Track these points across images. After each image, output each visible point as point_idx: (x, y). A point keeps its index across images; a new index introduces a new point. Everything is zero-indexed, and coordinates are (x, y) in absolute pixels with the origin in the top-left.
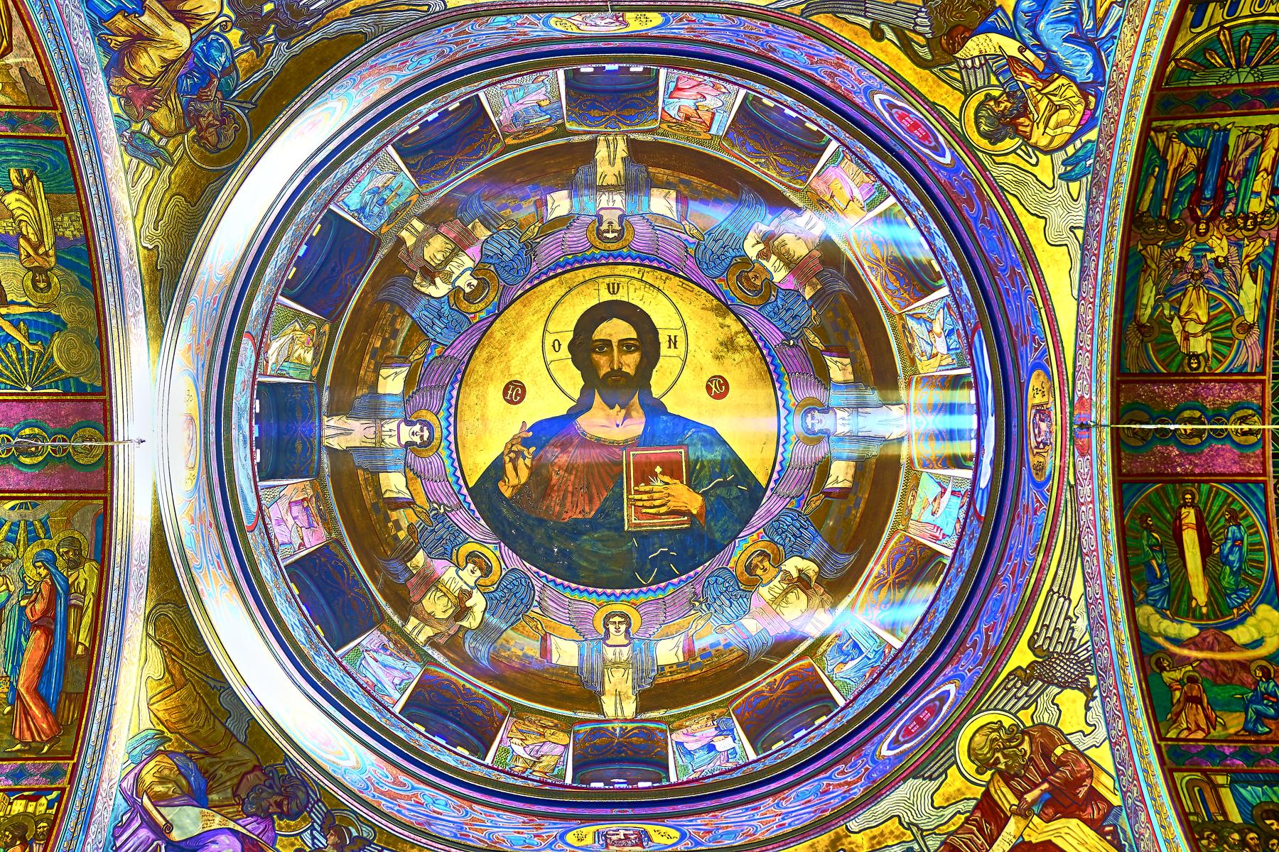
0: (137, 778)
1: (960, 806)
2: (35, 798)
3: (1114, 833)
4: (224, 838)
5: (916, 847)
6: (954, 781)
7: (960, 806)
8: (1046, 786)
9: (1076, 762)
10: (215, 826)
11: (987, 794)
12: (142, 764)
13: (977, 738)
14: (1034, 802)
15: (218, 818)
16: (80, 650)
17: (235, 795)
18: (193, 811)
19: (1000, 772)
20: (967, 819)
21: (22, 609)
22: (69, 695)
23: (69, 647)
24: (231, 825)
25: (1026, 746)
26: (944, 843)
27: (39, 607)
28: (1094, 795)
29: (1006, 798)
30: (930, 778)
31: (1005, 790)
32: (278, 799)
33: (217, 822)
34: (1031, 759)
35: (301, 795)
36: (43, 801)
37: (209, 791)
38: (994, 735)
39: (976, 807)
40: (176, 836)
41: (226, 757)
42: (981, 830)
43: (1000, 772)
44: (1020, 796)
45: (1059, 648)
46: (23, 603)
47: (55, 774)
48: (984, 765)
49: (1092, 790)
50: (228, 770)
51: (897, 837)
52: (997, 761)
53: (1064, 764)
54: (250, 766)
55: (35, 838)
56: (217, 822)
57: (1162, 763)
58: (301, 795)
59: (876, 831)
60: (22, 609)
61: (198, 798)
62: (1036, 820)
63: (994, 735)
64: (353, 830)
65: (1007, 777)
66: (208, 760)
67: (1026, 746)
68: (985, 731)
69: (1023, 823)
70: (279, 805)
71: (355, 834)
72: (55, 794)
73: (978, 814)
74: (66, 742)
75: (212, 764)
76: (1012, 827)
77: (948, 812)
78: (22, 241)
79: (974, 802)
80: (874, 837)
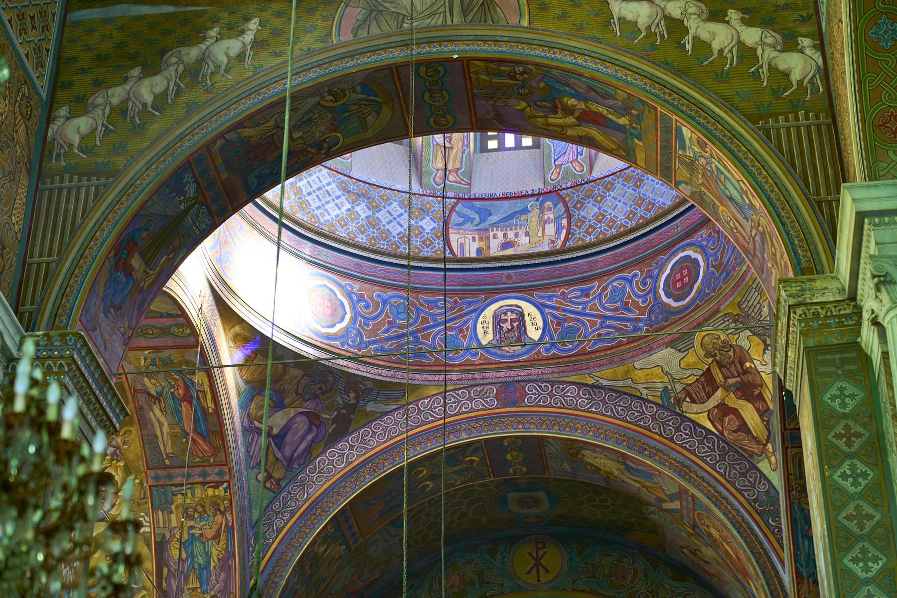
0: (249, 417)
1: (695, 372)
2: (216, 487)
3: (768, 422)
4: (298, 419)
5: (670, 387)
6: (691, 358)
7: (695, 372)
8: (739, 379)
9: (755, 375)
10: (292, 415)
11: (709, 369)
12: (249, 406)
13: (706, 338)
14: (732, 385)
15: (292, 411)
16: (210, 410)
17: (297, 394)
18: (279, 414)
19: (717, 361)
20: (697, 380)
21: (173, 393)
22: (213, 432)
23: (204, 410)
24: (300, 410)
25: (731, 353)
26: (684, 389)
27: (181, 392)
28: (761, 397)
29: (719, 377)
30: (679, 350)
31: (718, 371)
32: (319, 385)
33: (292, 412)
34: (733, 361)
35: (330, 379)
36: (221, 488)
37: (283, 399)
38: (715, 341)
39: (702, 375)
40: (275, 431)
41: (287, 377)
42: (704, 388)
43: (717, 361)
44: (726, 378)
45: (753, 314)
46: (172, 390)
47: (221, 474)
48: (708, 355)
49: (760, 393)
50: (290, 384)
51: (660, 378)
52: (715, 355)
53: (749, 373)
54: (300, 376)
55: (225, 510)
56: (292, 412)
57: (783, 443)
58: (330, 379)
59: (648, 371)
60: (173, 393)
61: (278, 405)
62: (732, 395)
63: (715, 341)
64: (361, 386)
65: (721, 366)
66: (279, 384)
67: (731, 353)
68: (711, 337)
69: (725, 394)
70: (321, 388)
71: (363, 387)
72: (226, 485)
73: (703, 379)
74: (221, 456)
75: (281, 385)
76: (719, 393)
77: (689, 372)
78: (166, 446)
79: (701, 372)
80: (648, 375)
